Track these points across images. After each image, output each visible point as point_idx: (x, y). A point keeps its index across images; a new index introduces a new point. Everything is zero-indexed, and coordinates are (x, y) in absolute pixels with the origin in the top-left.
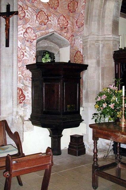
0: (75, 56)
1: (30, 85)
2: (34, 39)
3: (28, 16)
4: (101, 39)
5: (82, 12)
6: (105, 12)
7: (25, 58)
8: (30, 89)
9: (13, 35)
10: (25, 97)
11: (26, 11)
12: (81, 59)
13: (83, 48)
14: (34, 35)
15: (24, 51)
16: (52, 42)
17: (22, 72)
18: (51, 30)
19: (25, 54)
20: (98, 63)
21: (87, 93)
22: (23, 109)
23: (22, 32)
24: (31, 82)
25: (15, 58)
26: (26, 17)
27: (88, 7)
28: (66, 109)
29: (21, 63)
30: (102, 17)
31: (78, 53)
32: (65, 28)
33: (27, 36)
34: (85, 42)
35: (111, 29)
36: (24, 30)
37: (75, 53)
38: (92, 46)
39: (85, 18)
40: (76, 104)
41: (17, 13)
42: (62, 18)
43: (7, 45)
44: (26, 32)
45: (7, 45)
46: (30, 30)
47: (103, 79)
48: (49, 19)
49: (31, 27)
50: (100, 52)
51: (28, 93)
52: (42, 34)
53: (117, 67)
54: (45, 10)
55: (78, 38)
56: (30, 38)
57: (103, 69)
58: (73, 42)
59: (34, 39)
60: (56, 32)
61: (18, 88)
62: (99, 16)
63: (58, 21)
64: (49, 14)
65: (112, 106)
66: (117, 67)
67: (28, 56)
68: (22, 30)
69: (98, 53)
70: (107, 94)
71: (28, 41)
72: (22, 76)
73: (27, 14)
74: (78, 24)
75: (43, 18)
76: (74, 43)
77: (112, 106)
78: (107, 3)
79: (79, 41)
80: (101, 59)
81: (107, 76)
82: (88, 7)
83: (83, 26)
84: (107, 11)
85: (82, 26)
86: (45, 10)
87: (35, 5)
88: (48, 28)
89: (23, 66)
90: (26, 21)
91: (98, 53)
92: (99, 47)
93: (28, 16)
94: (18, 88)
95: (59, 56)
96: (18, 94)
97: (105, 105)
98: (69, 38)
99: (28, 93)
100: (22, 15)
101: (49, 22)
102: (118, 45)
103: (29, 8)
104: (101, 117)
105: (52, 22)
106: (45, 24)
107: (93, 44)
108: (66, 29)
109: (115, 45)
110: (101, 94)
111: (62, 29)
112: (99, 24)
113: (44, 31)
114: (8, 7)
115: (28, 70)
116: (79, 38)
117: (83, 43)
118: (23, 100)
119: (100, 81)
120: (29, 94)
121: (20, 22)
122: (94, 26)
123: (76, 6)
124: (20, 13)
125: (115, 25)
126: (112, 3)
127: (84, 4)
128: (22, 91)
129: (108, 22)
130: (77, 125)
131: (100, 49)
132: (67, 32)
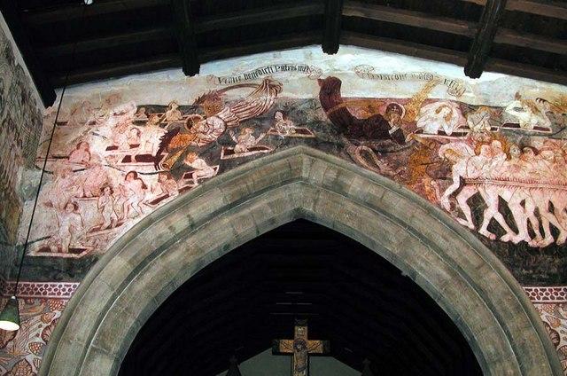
5: (30, 358)
43: (529, 221)
45: (529, 221)
127: (39, 340)
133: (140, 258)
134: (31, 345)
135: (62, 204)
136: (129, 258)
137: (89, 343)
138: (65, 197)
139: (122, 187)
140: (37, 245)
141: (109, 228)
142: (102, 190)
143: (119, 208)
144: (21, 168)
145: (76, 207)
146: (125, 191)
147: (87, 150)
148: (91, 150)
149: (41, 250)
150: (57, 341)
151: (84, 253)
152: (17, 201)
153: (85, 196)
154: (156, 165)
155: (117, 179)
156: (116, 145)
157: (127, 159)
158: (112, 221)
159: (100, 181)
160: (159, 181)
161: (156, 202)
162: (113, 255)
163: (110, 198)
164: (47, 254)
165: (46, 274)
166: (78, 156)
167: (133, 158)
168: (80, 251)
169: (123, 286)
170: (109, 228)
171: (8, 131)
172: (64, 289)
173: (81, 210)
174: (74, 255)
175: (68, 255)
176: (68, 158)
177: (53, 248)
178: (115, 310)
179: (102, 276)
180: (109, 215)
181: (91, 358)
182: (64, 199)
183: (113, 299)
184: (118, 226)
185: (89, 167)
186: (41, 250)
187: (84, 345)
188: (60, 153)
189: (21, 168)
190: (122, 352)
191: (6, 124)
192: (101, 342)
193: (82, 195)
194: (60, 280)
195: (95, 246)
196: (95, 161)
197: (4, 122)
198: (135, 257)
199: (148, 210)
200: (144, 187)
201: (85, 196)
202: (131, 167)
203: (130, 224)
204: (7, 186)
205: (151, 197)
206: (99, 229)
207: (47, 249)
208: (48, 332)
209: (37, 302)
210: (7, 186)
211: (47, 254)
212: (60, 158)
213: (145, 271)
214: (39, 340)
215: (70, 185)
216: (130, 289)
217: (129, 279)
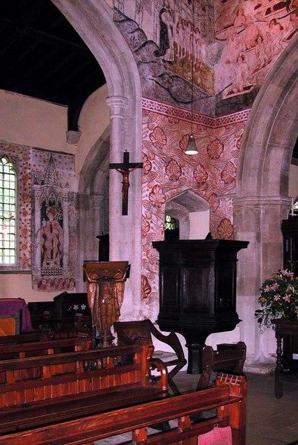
0: (219, 227)
1: (157, 272)
2: (162, 203)
3: (154, 168)
4: (263, 202)
5: (232, 160)
6: (269, 163)
7: (151, 231)
8: (157, 277)
9: (134, 198)
10: (150, 289)
11: (152, 162)
12: (230, 230)
13: (234, 215)
14: (163, 196)
15: (149, 221)
16: (180, 203)
17: (148, 252)
18: (184, 188)
19: (151, 225)
20: (258, 237)
21: (241, 280)
22: (148, 306)
23: (148, 193)
24: (158, 266)
25: (138, 232)
26: (152, 170)
27: (244, 155)
28: (219, 306)
29: (145, 239)
30: (263, 170)
31: (226, 221)
32: (204, 183)
33: (153, 198)
34: (237, 206)
35: (277, 188)
36: (150, 190)
37: (218, 222)
38: (249, 212)
39: (238, 170)
40: (231, 299)
41: (140, 165)
42: (199, 168)
43: (125, 212)
44: (153, 192)
45: (125, 212)
46: (158, 189)
47: (265, 261)
48: (183, 171)
49: (159, 184)
50: (261, 223)
51: (154, 283)
52: (173, 194)
53: (287, 243)
54: (177, 159)
55: (225, 200)
56: (157, 201)
57: (265, 246)
58: (216, 205)
59: (162, 203)
60: (191, 190)
61: (142, 276)
62: (260, 169)
63: (194, 173)
64: (182, 164)
65: (286, 298)
66: (287, 243)
67: (155, 228)
68: (148, 190)
69: (258, 222)
70: (279, 282)
71: (155, 206)
72: (147, 259)
73: (153, 165)
74: (224, 178)
75: (175, 169)
76: (218, 207)
77: (286, 298)
78: (273, 151)
79: (228, 203)
80: (262, 231)
81: (273, 257)
82: (244, 155)
83: (234, 182)
84: (273, 162)
85: (232, 182)
86: (177, 159)
87: (164, 151)
88: (181, 185)
89: (148, 243)
90: (152, 176)
91: (258, 222)
92: (259, 213)
93: (154, 168)
94: (142, 276)
95: (189, 225)
96: (142, 284)
97: (276, 298)
98: (209, 198)
99: (154, 283)
100: (147, 168)
101: (182, 176)
102: (288, 211)
103: (157, 158)
104: (267, 316)
105: (186, 174)
106: (177, 180)
107: (252, 210)
108: (205, 185)
109: (284, 212)
110: (269, 283)
111: (199, 184)
112: (259, 180)
113: (175, 190)
114: (126, 155)
115: (155, 249)
116: (227, 200)
117: (235, 207)
118: (148, 293)
119: (261, 263)
120: (155, 285)
121: (145, 178)
122: (252, 184)
123: (220, 150)
124: (145, 164)
125: (284, 181)
126: (280, 151)
127: (235, 149)
128: (147, 281)
129: (274, 177)
130: (231, 328)
131: (261, 216)
132: (206, 189)
133: (286, 80)
134: (232, 153)
135: (235, 59)
136: (278, 82)
137: (266, 142)
138: (236, 53)
139: (268, 34)
140: (226, 91)
141: (264, 66)
142: (256, 40)
143: (268, 50)
144: (203, 46)
145: (243, 59)
146: (270, 36)
147: (243, 15)
148: (245, 14)
149: (229, 94)
150: (244, 147)
151: (252, 88)
152: (207, 68)
153: (247, 49)
154: (288, 9)
155: (264, 28)
156: (260, 3)
157: (268, 11)
158: (265, 60)
159: (254, 34)
160: (291, 20)
161: (289, 38)
162: (267, 84)
163: (262, 44)
164: (232, 95)
165: (234, 108)
166: (238, 22)
167: (272, 9)
168: (248, 88)
169: (279, 102)
170: (264, 66)
171: (183, 29)
172: (244, 115)
173: (246, 59)
174: (247, 91)
175: (243, 92)
176: (233, 25)
177: (235, 90)
178: (278, 118)
179: (264, 100)
180: (263, 57)
181: (268, 152)
182: (236, 55)
183: (275, 112)
184: (269, 62)
185: (246, 26)
186: (229, 94)
187: (261, 145)
188: (228, 23)
189: (203, 46)
190: (290, 145)
191: (180, 25)
192: (273, 140)
193: (245, 49)
194: (240, 110)
195: (257, 81)
196: (249, 20)
197: (178, 24)
198: (282, 81)
199: (285, 45)
200: (282, 28)
201: (247, 49)
202: (271, 17)
203: (275, 59)
204: (195, 62)
205: (286, 35)
206: (258, 70)
207: (231, 92)
208: (239, 143)
209: (231, 127)
210: (195, 62)
211: (232, 95)
212: (229, 26)
213: (294, 87)
214: (235, 149)
215: (237, 45)
216: (285, 103)
217: (282, 96)
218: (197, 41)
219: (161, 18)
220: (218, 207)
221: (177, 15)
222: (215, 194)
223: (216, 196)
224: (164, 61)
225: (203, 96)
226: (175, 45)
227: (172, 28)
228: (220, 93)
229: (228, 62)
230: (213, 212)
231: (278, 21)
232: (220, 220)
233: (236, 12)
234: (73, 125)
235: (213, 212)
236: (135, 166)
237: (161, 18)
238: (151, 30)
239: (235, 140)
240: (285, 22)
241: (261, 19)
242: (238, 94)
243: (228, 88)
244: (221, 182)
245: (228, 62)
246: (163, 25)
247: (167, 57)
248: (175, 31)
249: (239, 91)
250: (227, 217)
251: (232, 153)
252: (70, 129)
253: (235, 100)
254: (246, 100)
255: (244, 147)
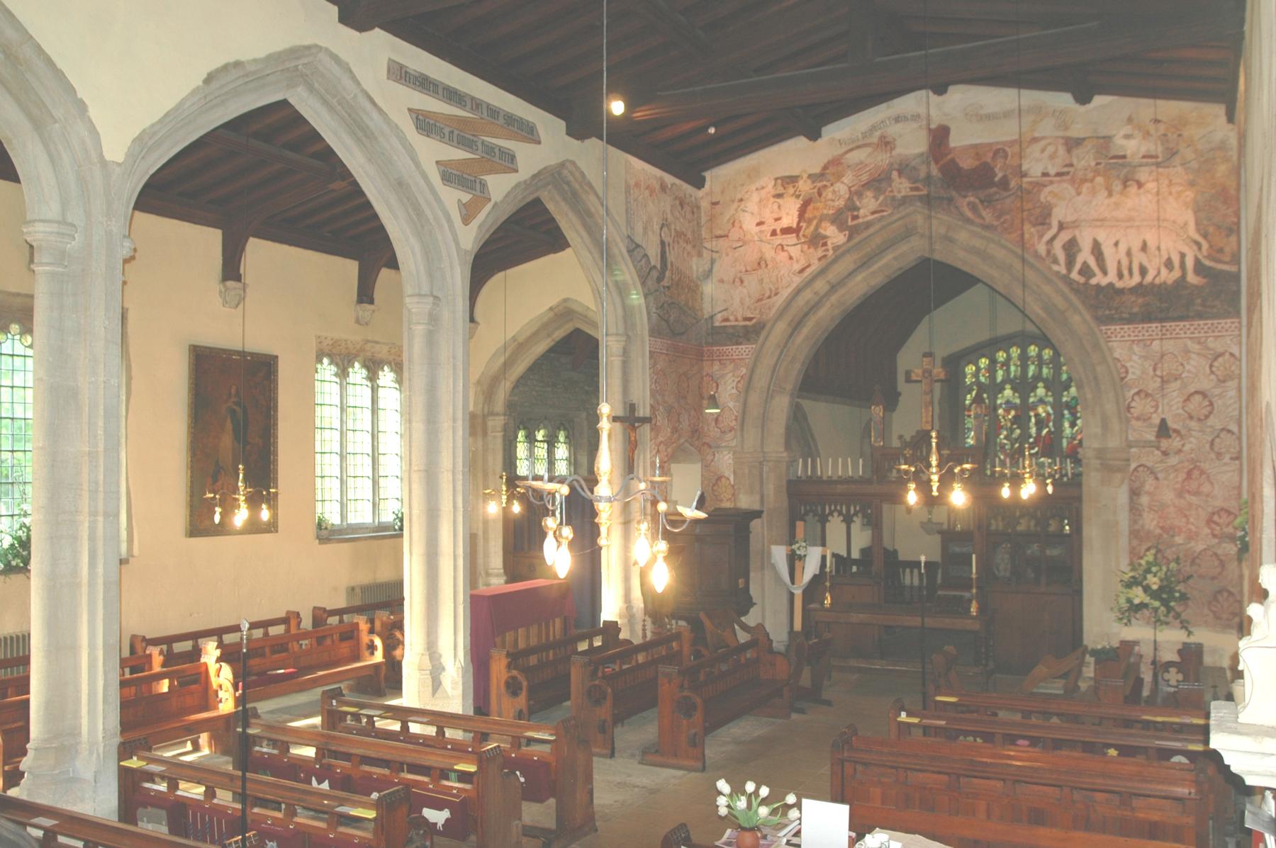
13: (735, 473)
30: (764, 420)
31: (723, 480)
35: (782, 441)
44: (658, 451)
54: (676, 405)
73: (659, 418)
76: (712, 461)
83: (733, 432)
85: (731, 431)
116: (725, 453)
134: (729, 395)
135: (731, 279)
139: (773, 259)
140: (719, 317)
142: (759, 264)
145: (742, 282)
147: (741, 227)
153: (747, 271)
155: (769, 253)
156: (763, 220)
158: (771, 290)
161: (802, 271)
166: (735, 234)
168: (750, 319)
170: (769, 297)
173: (746, 283)
176: (727, 236)
177: (732, 318)
185: (745, 243)
193: (744, 270)
194: (741, 344)
200: (791, 258)
205: (797, 267)
207: (727, 320)
208: (739, 385)
214: (734, 391)
217: (791, 335)
218: (688, 253)
219: (661, 235)
220: (712, 461)
221: (673, 227)
222: (707, 444)
223: (710, 447)
224: (664, 287)
225: (694, 321)
226: (672, 263)
227: (669, 245)
228: (712, 317)
229: (722, 281)
230: (706, 466)
231: (786, 248)
232: (716, 477)
233: (731, 221)
234: (365, 294)
235: (706, 466)
236: (644, 420)
237: (661, 235)
238: (653, 252)
239: (733, 381)
240: (795, 251)
241: (764, 238)
242: (736, 323)
243: (723, 313)
244: (716, 429)
245: (722, 281)
246: (663, 243)
247: (666, 283)
248: (671, 247)
249: (736, 320)
250: (726, 475)
251: (729, 395)
252: (361, 300)
253: (731, 331)
254: (750, 332)
255: (747, 391)
